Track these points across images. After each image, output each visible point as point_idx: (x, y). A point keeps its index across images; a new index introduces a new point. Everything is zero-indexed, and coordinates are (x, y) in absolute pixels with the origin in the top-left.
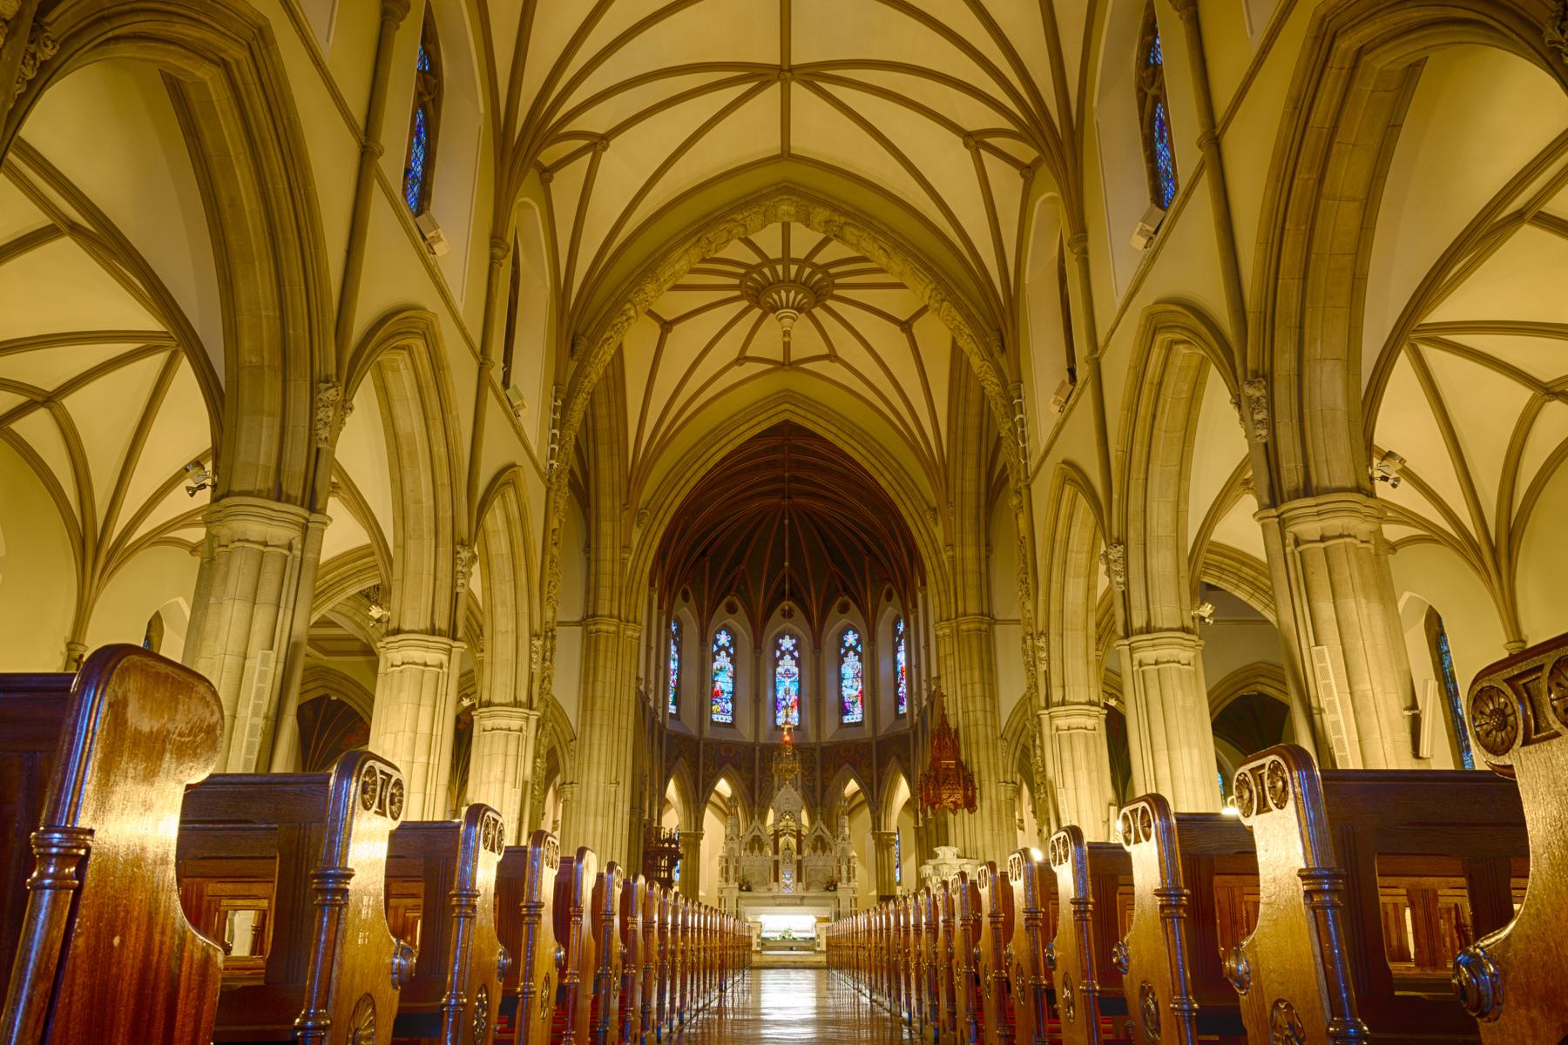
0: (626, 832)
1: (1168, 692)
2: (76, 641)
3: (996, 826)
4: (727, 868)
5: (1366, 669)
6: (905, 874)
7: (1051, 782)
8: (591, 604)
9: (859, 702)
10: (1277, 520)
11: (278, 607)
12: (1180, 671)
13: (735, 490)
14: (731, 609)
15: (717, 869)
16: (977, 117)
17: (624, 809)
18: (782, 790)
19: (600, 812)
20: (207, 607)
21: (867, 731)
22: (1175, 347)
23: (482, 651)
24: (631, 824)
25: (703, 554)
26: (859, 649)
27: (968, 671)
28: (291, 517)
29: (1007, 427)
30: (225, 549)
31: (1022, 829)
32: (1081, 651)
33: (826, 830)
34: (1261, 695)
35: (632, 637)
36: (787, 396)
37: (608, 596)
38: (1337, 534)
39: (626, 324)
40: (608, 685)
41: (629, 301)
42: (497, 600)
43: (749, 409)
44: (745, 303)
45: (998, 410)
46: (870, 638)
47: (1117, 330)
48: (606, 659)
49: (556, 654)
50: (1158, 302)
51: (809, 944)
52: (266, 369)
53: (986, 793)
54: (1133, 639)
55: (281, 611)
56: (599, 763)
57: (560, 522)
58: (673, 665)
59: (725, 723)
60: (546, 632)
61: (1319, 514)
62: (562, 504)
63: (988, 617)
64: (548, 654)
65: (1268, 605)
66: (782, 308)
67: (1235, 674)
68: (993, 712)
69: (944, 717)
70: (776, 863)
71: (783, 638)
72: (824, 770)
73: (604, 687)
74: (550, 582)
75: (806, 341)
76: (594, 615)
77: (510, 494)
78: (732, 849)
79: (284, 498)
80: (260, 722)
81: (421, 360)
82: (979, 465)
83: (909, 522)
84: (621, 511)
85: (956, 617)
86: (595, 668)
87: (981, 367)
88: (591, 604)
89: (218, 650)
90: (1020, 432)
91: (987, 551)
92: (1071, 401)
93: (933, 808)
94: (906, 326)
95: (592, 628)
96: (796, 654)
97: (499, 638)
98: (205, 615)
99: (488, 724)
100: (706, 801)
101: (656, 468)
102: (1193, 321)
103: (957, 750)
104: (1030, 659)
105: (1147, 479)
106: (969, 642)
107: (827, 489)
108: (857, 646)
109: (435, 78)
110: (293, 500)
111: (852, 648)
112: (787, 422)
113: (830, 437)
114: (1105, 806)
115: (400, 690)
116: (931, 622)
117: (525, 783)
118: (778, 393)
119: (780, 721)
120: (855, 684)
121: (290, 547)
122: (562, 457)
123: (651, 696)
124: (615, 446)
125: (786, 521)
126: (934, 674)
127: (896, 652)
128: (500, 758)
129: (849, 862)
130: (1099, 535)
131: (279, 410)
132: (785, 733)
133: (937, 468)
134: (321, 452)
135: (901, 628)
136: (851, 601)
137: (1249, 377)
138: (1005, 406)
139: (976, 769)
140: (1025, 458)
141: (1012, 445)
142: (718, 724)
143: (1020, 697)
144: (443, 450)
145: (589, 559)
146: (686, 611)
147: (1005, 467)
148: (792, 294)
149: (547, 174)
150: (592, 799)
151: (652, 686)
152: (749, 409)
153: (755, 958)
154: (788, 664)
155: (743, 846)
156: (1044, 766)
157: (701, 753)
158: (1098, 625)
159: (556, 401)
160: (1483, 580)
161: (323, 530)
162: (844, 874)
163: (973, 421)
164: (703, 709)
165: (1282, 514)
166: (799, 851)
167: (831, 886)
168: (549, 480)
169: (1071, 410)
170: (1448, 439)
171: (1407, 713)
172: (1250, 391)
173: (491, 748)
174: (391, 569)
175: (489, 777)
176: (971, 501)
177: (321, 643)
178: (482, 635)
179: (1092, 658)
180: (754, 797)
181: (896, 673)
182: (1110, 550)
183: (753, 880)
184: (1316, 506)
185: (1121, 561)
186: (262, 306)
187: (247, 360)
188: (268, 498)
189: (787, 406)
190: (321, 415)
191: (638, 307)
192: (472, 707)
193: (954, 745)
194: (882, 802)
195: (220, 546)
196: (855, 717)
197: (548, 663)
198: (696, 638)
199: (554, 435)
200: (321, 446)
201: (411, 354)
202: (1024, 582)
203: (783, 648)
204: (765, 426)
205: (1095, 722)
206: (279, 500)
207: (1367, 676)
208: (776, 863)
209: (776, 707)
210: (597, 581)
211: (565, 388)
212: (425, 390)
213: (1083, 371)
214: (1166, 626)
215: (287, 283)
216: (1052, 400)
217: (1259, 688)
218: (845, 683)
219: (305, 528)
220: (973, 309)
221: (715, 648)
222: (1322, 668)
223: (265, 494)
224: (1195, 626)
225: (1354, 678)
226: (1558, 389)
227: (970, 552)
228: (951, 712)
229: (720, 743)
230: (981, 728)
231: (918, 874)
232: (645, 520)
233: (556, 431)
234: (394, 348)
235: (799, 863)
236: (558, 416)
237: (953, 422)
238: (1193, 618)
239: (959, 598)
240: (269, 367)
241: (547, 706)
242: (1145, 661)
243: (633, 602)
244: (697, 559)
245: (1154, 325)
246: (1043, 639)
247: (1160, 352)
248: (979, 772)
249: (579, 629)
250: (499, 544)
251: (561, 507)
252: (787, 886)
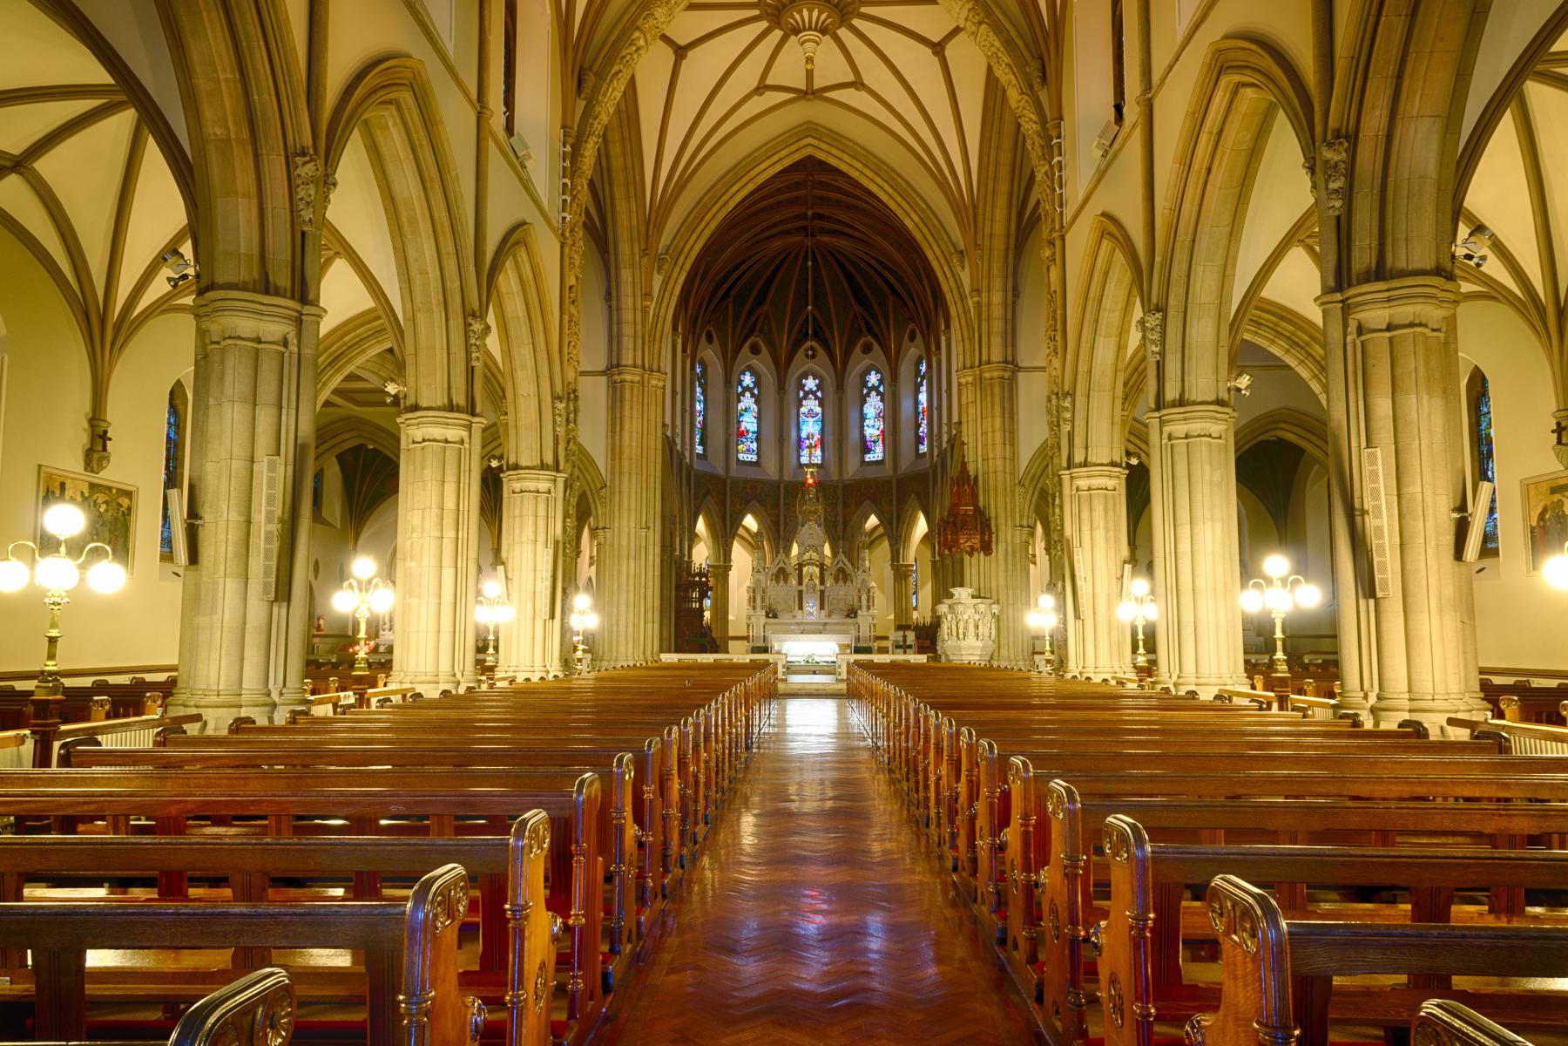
0: (658, 573)
1: (1196, 467)
2: (97, 417)
3: (1010, 567)
4: (754, 598)
5: (1419, 470)
7: (1068, 541)
8: (615, 353)
9: (880, 441)
10: (1340, 305)
11: (280, 407)
13: (758, 229)
14: (755, 350)
15: (745, 596)
17: (655, 552)
18: (806, 526)
19: (632, 554)
20: (207, 407)
21: (888, 470)
22: (1242, 90)
23: (506, 414)
24: (662, 561)
25: (726, 294)
26: (881, 389)
27: (990, 419)
28: (282, 310)
29: (1043, 171)
30: (218, 346)
31: (1034, 563)
32: (1106, 411)
33: (847, 563)
34: (1280, 440)
35: (656, 386)
36: (809, 129)
37: (631, 346)
38: (1407, 322)
39: (635, 56)
40: (634, 434)
41: (638, 28)
42: (517, 363)
43: (771, 144)
44: (764, 24)
45: (1034, 147)
46: (892, 379)
47: (1176, 66)
48: (631, 408)
49: (580, 415)
50: (1226, 37)
51: (829, 669)
52: (233, 143)
53: (1002, 536)
55: (284, 412)
56: (629, 510)
57: (577, 279)
58: (699, 407)
59: (750, 462)
60: (569, 394)
61: (1389, 300)
62: (577, 260)
63: (1012, 364)
64: (572, 416)
65: (1302, 362)
66: (805, 30)
67: (1257, 420)
68: (1012, 459)
69: (964, 464)
70: (800, 593)
71: (807, 379)
72: (846, 505)
73: (631, 437)
74: (570, 342)
75: (830, 67)
76: (618, 365)
78: (759, 580)
79: (272, 290)
80: (275, 527)
81: (410, 114)
82: (1010, 206)
83: (935, 264)
84: (640, 258)
85: (980, 365)
86: (621, 418)
87: (1020, 101)
88: (615, 353)
89: (224, 455)
90: (1056, 178)
91: (1013, 296)
92: (1116, 146)
93: (950, 550)
94: (938, 48)
95: (618, 378)
96: (819, 394)
97: (521, 402)
98: (206, 414)
99: (517, 486)
100: (733, 535)
101: (673, 213)
102: (1268, 63)
103: (975, 496)
104: (1055, 419)
105: (1194, 240)
106: (992, 389)
107: (850, 226)
108: (879, 386)
110: (282, 292)
111: (874, 388)
112: (810, 158)
113: (855, 174)
114: (1119, 564)
115: (423, 467)
116: (954, 368)
117: (556, 543)
118: (800, 125)
119: (804, 460)
120: (877, 424)
121: (285, 343)
122: (574, 208)
123: (678, 440)
124: (631, 187)
125: (810, 263)
126: (955, 419)
127: (917, 392)
128: (531, 519)
129: (869, 591)
130: (1135, 292)
131: (254, 190)
132: (809, 476)
133: (966, 208)
134: (306, 235)
135: (923, 368)
136: (873, 340)
137: (1329, 137)
138: (1043, 146)
139: (993, 514)
140: (1061, 206)
141: (1048, 191)
142: (744, 463)
143: (1042, 442)
144: (445, 215)
145: (610, 307)
146: (710, 353)
147: (1038, 202)
148: (815, 13)
150: (624, 543)
151: (678, 431)
152: (771, 144)
153: (781, 687)
154: (811, 404)
155: (769, 577)
156: (1062, 525)
157: (728, 489)
158: (1125, 384)
159: (565, 147)
160: (1543, 346)
161: (318, 323)
162: (864, 602)
163: (1005, 157)
164: (729, 450)
165: (1347, 299)
166: (822, 582)
167: (852, 613)
168: (563, 235)
169: (1115, 156)
170: (1533, 189)
171: (1456, 515)
172: (1328, 154)
173: (521, 509)
174: (404, 342)
175: (521, 537)
176: (999, 244)
177: (350, 394)
178: (505, 398)
179: (1118, 418)
180: (779, 532)
181: (917, 414)
182: (1147, 318)
183: (779, 608)
184: (1387, 291)
185: (1158, 329)
186: (219, 68)
187: (211, 131)
188: (255, 291)
189: (810, 140)
190: (301, 194)
191: (648, 35)
192: (500, 469)
193: (973, 491)
194: (901, 536)
195: (212, 343)
196: (876, 455)
197: (572, 425)
198: (721, 379)
199: (565, 185)
200: (305, 229)
201: (399, 108)
202: (1052, 339)
203: (806, 389)
204: (787, 162)
205: (1115, 482)
206: (267, 292)
207: (1418, 477)
208: (800, 593)
209: (799, 446)
210: (619, 330)
211: (574, 132)
212: (419, 150)
213: (1132, 112)
214: (1200, 399)
215: (242, 38)
216: (1096, 143)
217: (1280, 433)
218: (867, 422)
219: (299, 322)
220: (1013, 34)
221: (740, 389)
222: (1372, 471)
223: (251, 286)
224: (1230, 398)
225: (1405, 480)
227: (997, 297)
228: (971, 460)
229: (746, 481)
230: (1000, 475)
231: (934, 610)
232: (666, 267)
233: (567, 181)
234: (380, 103)
235: (822, 592)
236: (568, 164)
237: (985, 157)
238: (1229, 390)
239: (983, 345)
240: (237, 140)
241: (574, 467)
242: (1081, 488)
243: (656, 351)
244: (720, 301)
245: (1220, 65)
246: (1069, 399)
247: (1224, 96)
248: (996, 517)
249: (604, 379)
250: (515, 306)
251: (577, 263)
252: (811, 614)
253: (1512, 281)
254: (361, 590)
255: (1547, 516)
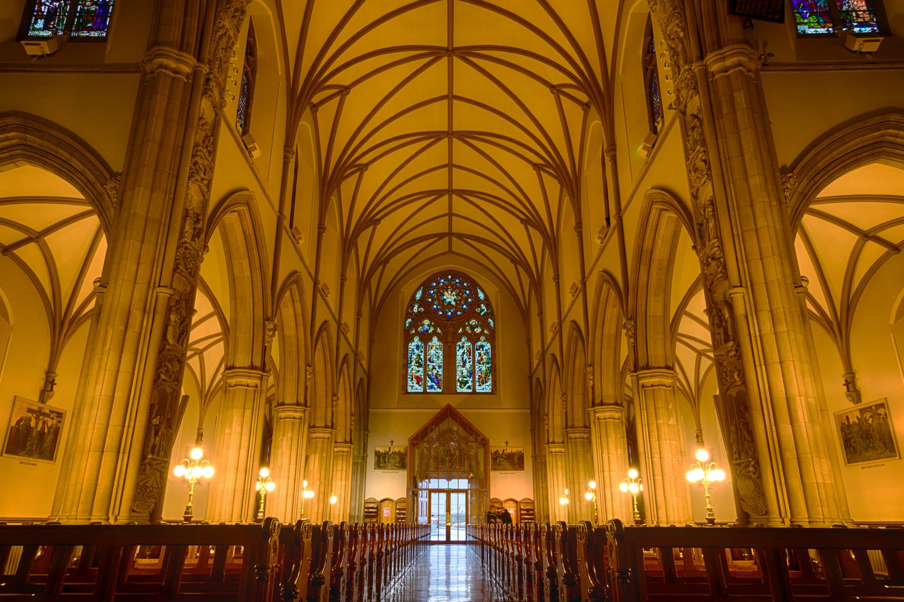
6: (738, 383)
12: (583, 442)
16: (558, 78)
50: (653, 188)
54: (595, 408)
77: (294, 287)
99: (283, 415)
109: (253, 58)
121: (256, 386)
149: (315, 108)
169: (656, 154)
213: (613, 222)
226: (871, 235)
242: (600, 418)
253: (826, 306)
254: (262, 482)
255: (21, 423)
